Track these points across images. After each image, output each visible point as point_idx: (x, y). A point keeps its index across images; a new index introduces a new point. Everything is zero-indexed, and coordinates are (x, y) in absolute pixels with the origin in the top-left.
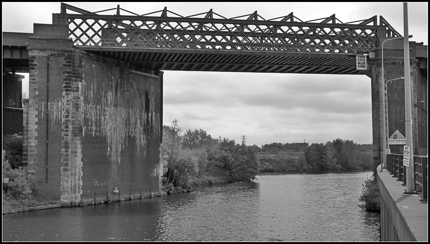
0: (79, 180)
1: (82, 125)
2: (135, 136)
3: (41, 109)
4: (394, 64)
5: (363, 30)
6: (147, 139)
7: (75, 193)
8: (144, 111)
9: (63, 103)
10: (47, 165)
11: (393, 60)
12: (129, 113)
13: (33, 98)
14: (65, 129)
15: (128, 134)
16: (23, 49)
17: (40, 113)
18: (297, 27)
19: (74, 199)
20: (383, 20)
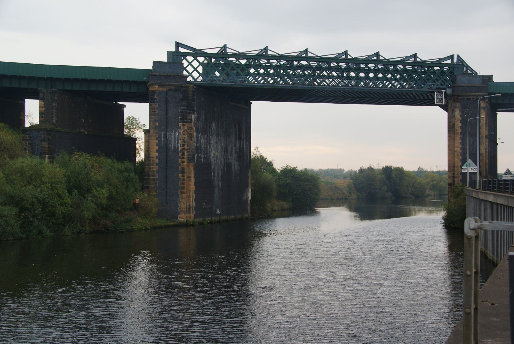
0: (192, 202)
1: (195, 153)
2: (231, 163)
3: (161, 138)
4: (468, 99)
5: (404, 66)
6: (239, 165)
7: (190, 213)
8: (237, 139)
9: (180, 133)
10: (167, 188)
11: (468, 96)
12: (227, 142)
13: (154, 128)
14: (181, 157)
15: (226, 160)
16: (144, 83)
17: (160, 141)
18: (203, 57)
19: (189, 218)
20: (460, 58)
